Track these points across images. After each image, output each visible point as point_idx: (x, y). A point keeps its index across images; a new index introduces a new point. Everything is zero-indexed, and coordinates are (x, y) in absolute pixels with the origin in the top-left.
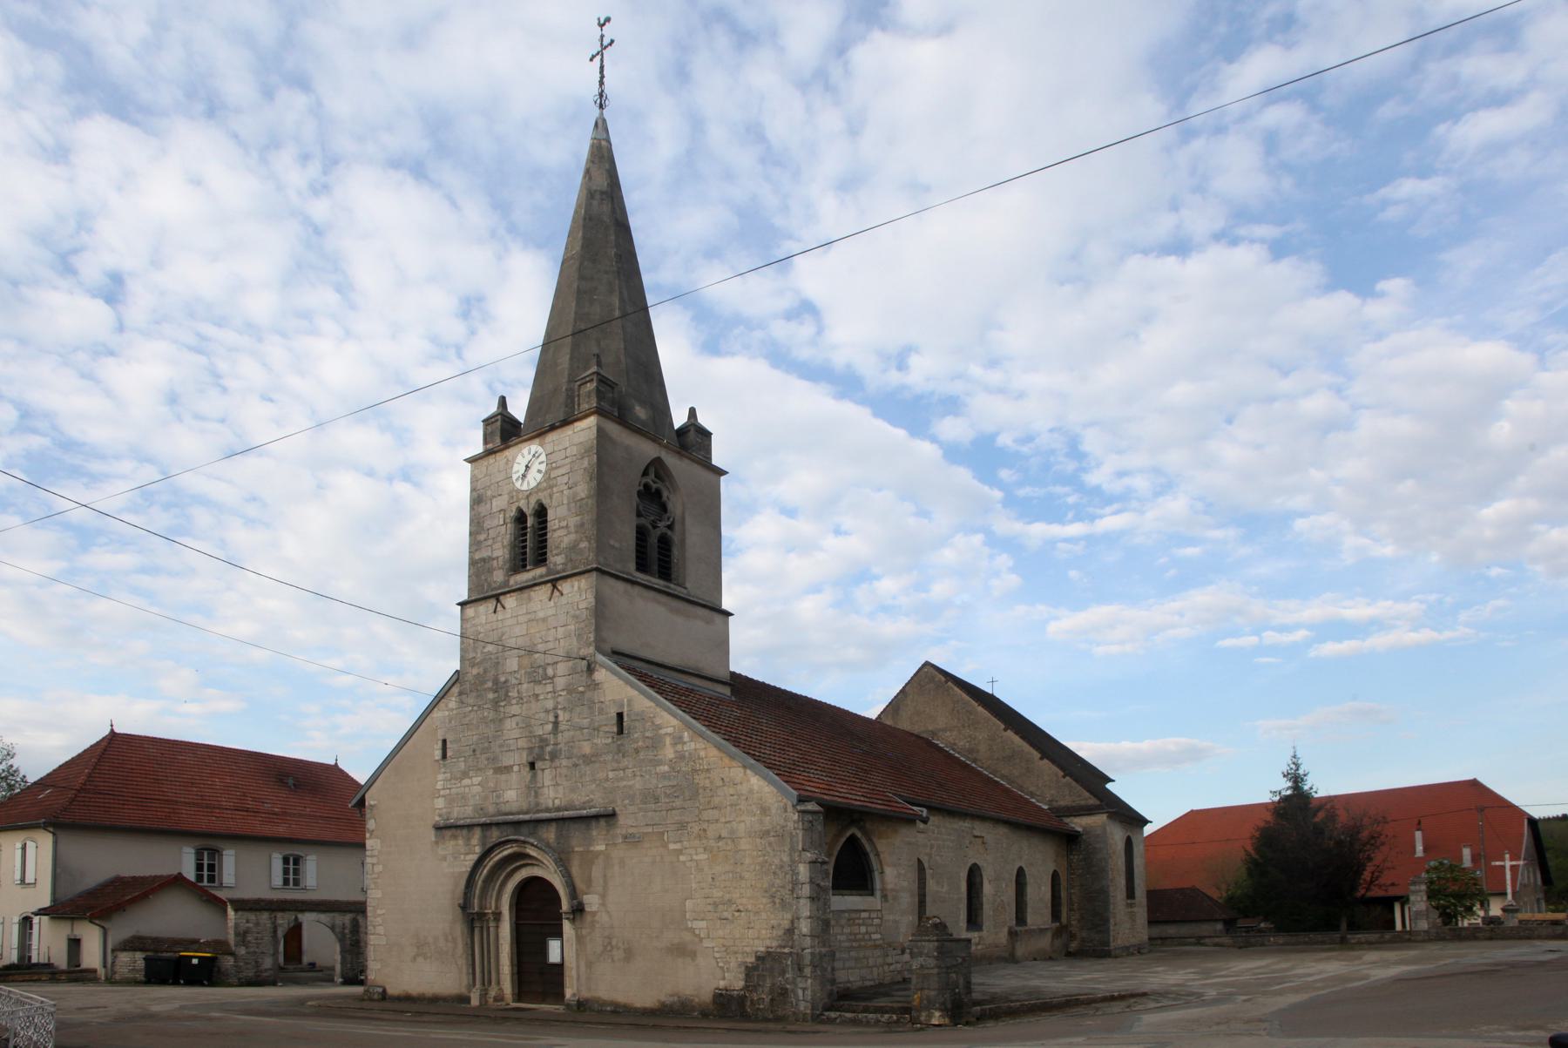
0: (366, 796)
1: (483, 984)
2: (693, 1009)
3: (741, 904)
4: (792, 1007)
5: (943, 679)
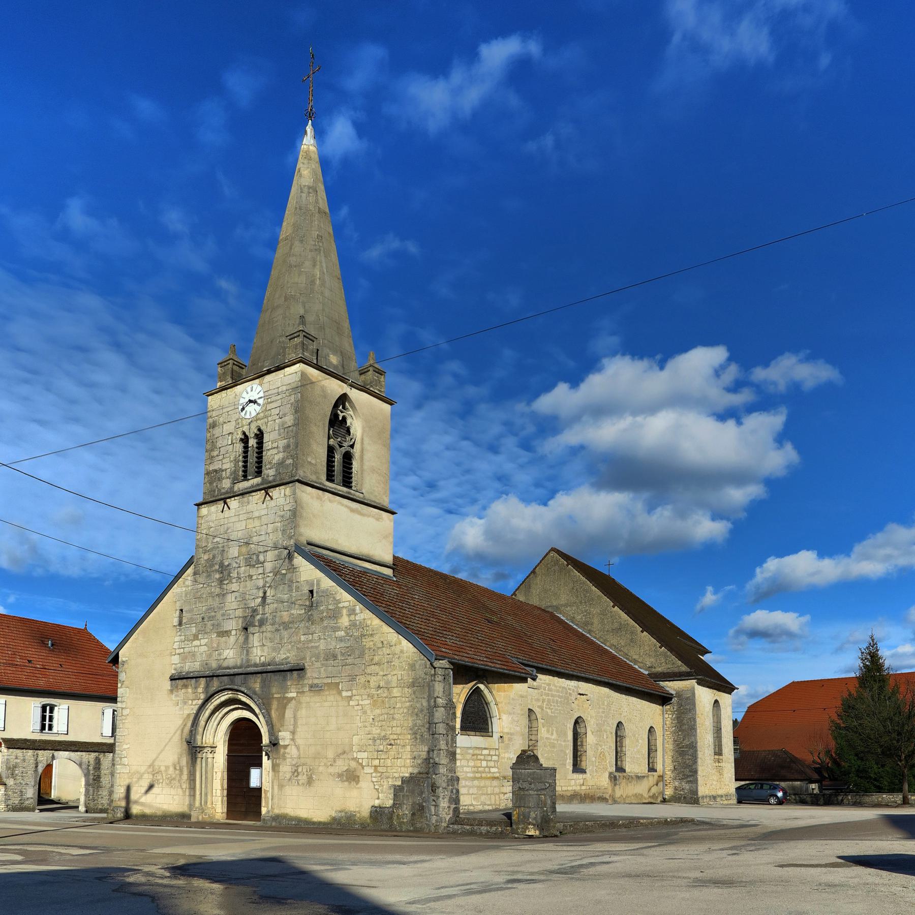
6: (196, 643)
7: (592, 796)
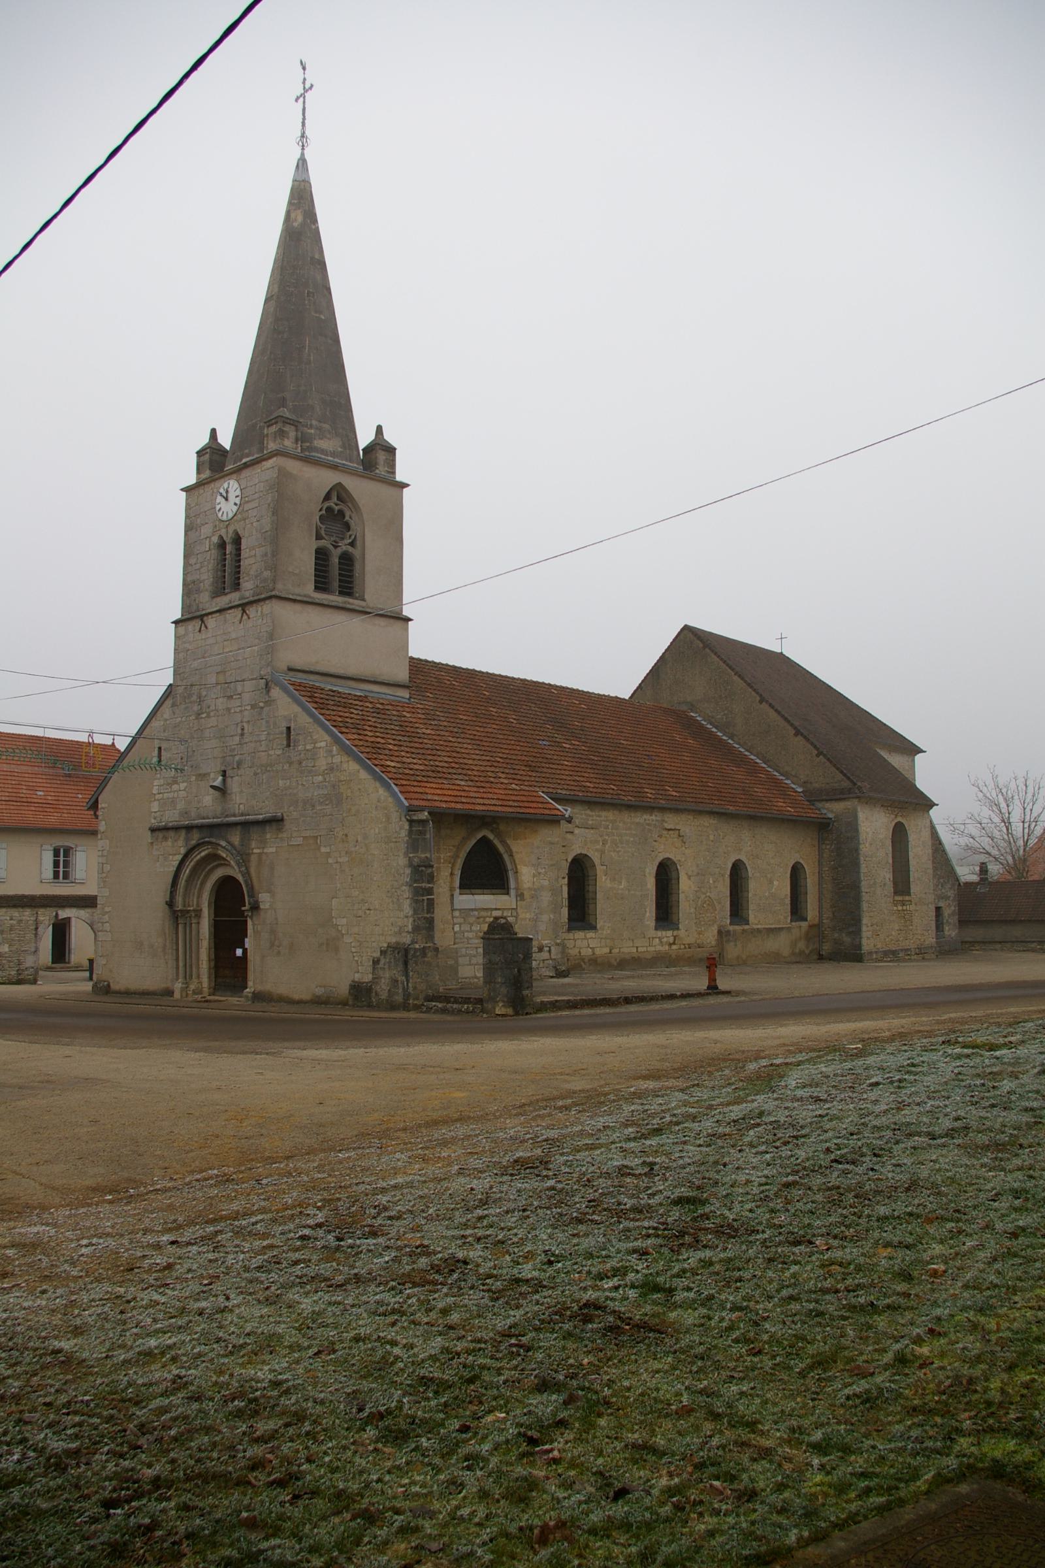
1: (185, 978)
5: (701, 645)
6: (175, 787)
7: (689, 958)
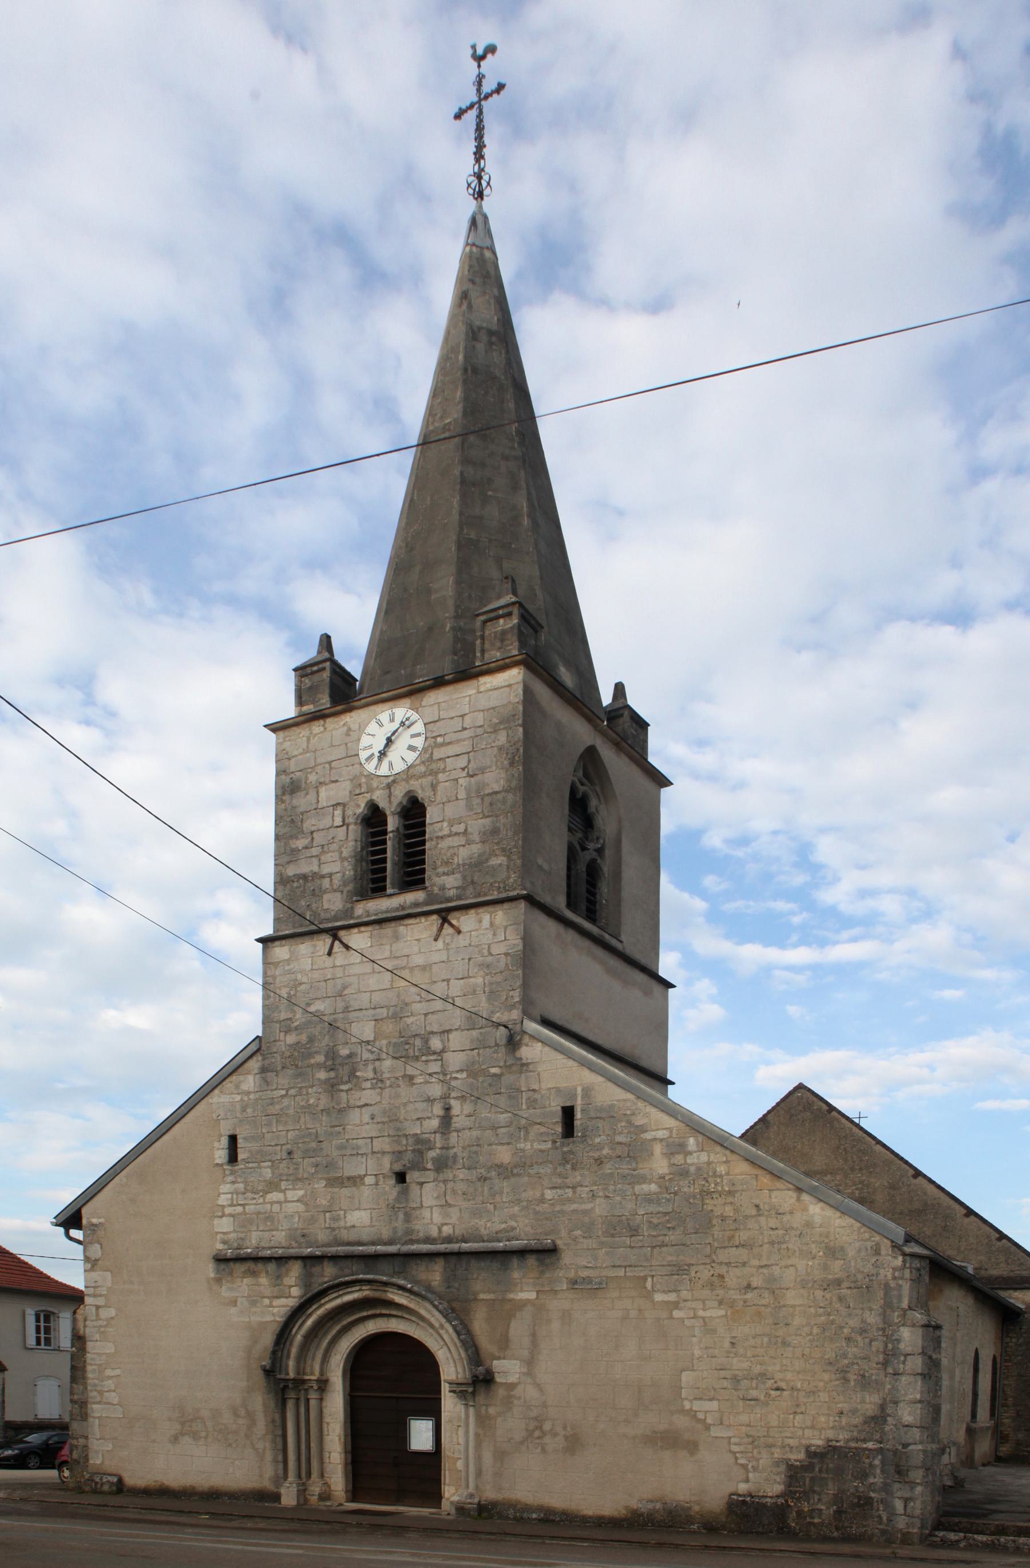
0: (84, 1211)
1: (299, 1477)
2: (690, 1520)
3: (781, 1380)
4: (880, 1522)
